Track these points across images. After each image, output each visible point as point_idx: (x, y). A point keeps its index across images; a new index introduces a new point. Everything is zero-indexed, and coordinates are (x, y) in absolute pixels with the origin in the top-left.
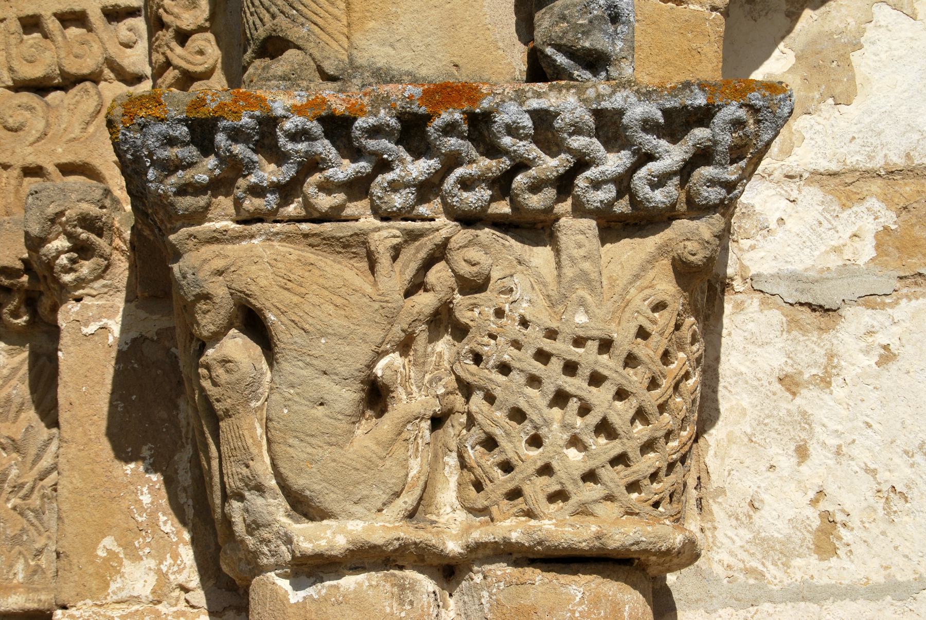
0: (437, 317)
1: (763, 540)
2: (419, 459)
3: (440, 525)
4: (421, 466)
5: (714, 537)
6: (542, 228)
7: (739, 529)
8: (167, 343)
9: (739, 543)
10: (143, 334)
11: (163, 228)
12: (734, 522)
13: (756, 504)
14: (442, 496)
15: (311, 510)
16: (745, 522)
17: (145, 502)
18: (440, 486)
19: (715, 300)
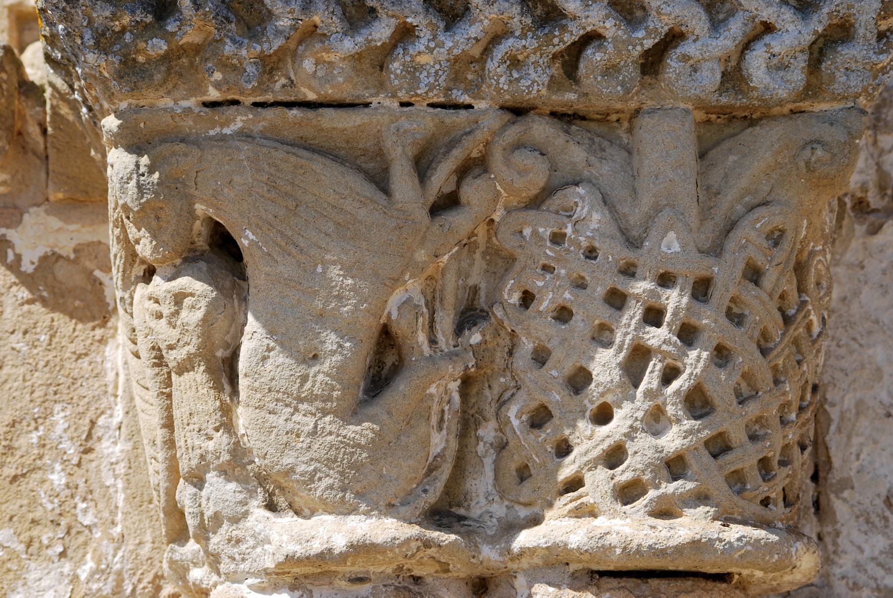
0: (473, 239)
2: (444, 432)
3: (471, 523)
4: (447, 441)
5: (835, 544)
6: (618, 120)
7: (870, 534)
8: (89, 265)
9: (867, 553)
10: (56, 250)
11: (96, 107)
12: (865, 527)
14: (474, 482)
15: (296, 499)
17: (56, 483)
18: (471, 470)
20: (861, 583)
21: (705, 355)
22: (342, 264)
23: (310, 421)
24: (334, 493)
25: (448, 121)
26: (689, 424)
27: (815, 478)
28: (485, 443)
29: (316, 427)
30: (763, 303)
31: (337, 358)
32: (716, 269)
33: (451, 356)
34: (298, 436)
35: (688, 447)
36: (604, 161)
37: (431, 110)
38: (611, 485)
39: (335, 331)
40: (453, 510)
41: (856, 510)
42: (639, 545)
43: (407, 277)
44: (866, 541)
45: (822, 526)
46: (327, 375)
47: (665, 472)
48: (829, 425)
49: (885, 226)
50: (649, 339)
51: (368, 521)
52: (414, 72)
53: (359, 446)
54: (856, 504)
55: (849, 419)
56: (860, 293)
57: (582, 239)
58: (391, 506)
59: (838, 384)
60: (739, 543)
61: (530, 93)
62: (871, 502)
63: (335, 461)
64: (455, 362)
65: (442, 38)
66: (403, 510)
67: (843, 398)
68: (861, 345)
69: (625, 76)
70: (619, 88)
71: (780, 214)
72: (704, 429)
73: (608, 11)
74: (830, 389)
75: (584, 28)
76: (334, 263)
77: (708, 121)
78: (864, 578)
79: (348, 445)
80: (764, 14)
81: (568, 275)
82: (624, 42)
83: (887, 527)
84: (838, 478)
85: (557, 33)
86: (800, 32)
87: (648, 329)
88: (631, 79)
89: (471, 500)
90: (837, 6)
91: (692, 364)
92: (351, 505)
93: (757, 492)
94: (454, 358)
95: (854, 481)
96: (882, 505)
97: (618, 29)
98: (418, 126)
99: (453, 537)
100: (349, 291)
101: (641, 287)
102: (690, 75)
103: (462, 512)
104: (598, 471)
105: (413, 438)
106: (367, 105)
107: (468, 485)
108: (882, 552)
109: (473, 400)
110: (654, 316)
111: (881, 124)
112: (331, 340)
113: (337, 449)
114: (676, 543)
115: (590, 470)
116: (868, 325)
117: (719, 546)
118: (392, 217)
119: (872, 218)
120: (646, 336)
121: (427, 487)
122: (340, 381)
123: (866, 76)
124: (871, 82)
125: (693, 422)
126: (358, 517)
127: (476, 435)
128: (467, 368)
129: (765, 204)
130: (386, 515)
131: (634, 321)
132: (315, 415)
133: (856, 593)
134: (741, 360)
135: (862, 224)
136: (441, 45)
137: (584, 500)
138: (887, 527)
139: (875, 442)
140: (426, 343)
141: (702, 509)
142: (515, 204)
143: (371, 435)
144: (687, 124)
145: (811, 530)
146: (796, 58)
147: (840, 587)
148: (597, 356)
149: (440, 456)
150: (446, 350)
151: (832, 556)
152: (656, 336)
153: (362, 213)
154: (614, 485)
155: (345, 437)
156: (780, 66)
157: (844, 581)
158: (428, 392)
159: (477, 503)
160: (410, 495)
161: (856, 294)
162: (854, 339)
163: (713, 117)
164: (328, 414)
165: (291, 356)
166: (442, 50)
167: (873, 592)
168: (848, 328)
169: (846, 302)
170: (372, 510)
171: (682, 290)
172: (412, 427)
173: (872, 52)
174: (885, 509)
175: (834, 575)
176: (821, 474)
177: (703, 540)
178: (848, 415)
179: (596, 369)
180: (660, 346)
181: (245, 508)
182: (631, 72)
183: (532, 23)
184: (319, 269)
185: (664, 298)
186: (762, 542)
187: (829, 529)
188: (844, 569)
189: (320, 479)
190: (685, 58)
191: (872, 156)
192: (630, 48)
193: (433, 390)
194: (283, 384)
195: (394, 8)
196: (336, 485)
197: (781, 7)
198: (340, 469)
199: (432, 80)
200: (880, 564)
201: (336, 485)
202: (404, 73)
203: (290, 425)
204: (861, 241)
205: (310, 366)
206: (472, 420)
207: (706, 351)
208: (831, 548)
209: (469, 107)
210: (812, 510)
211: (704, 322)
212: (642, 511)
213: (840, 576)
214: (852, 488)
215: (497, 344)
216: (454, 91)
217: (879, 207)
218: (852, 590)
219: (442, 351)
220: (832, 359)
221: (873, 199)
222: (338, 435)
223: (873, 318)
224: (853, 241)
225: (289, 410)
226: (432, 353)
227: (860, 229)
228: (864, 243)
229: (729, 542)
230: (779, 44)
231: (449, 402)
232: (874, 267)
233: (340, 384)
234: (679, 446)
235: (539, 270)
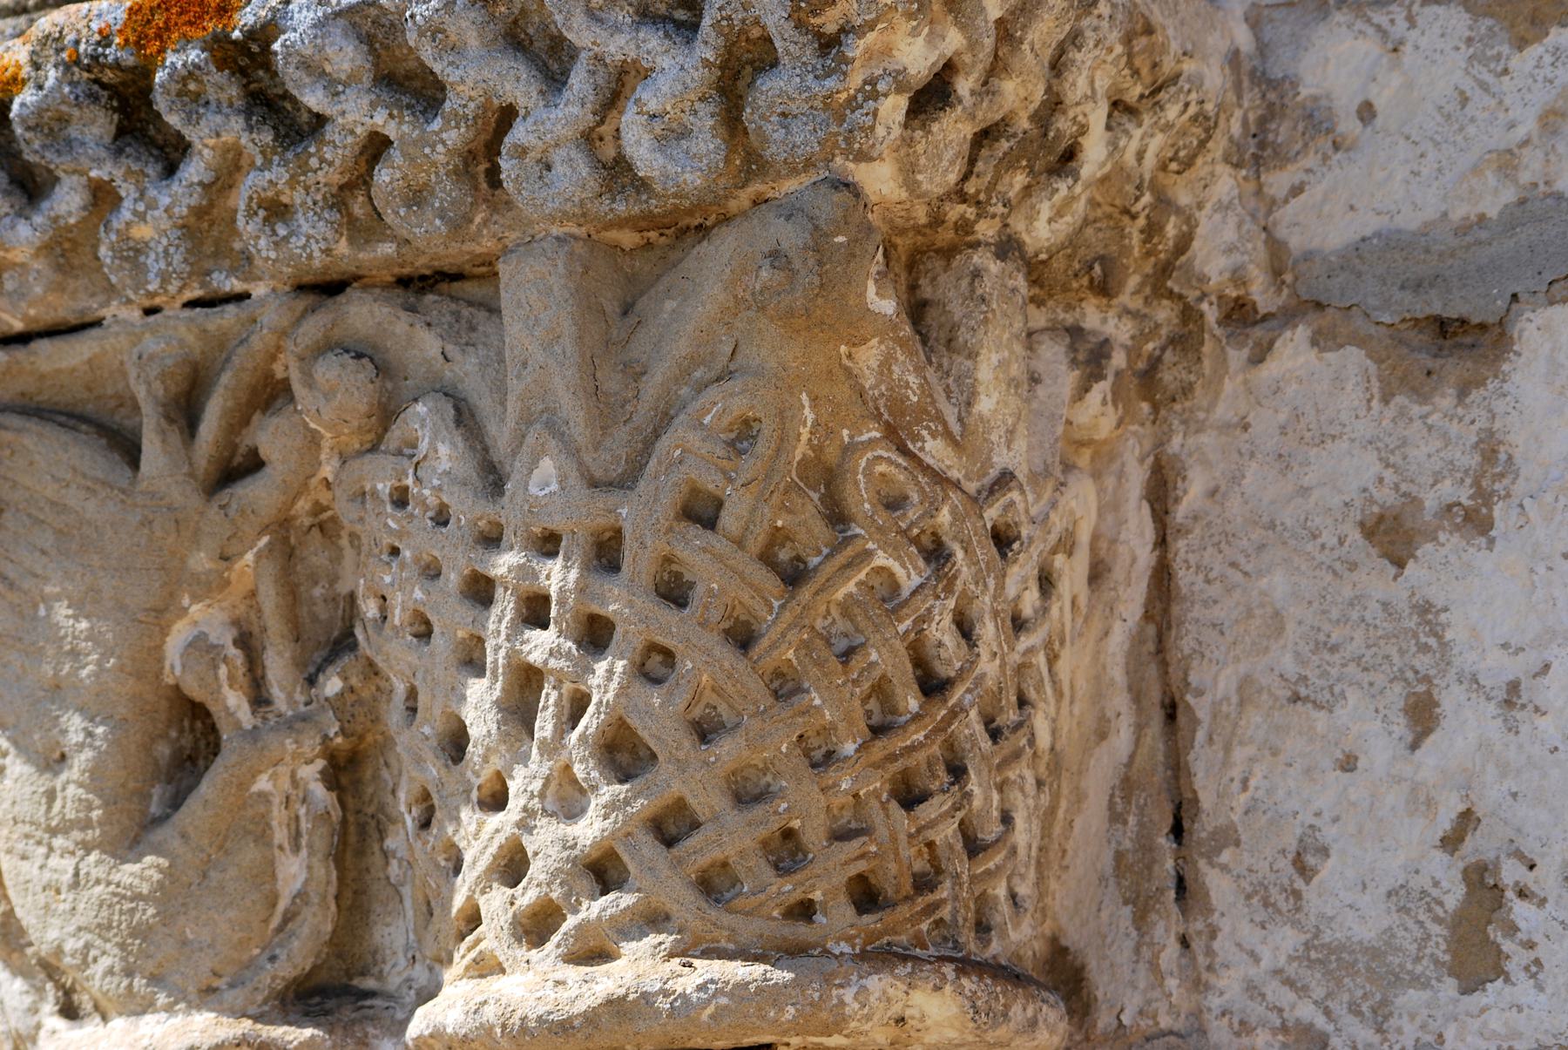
1: (1330, 949)
2: (304, 852)
4: (309, 868)
5: (1210, 952)
13: (1311, 860)
14: (387, 930)
16: (1284, 909)
19: (1202, 343)
20: (1253, 1021)
21: (620, 665)
22: (69, 598)
23: (68, 864)
24: (116, 980)
25: (211, 327)
26: (610, 791)
27: (1178, 831)
28: (400, 860)
29: (77, 874)
30: (719, 558)
31: (88, 754)
32: (624, 512)
33: (291, 725)
34: (58, 892)
35: (613, 833)
36: (471, 349)
37: (188, 313)
38: (510, 914)
39: (81, 710)
40: (355, 982)
41: (1244, 884)
42: (524, 1019)
43: (186, 601)
44: (1264, 941)
45: (1186, 921)
46: (80, 785)
47: (586, 883)
48: (1194, 731)
49: (1278, 344)
50: (529, 653)
51: (173, 1021)
52: (136, 257)
53: (138, 897)
54: (1246, 873)
55: (1227, 716)
56: (1244, 477)
57: (427, 492)
58: (211, 990)
59: (1207, 653)
60: (702, 995)
61: (310, 257)
62: (1271, 865)
63: (110, 927)
64: (299, 732)
65: (152, 193)
66: (229, 996)
67: (1215, 680)
68: (1246, 574)
69: (442, 200)
70: (438, 222)
71: (743, 392)
72: (635, 798)
73: (373, 97)
74: (1195, 663)
75: (352, 132)
76: (58, 598)
77: (649, 245)
78: (1261, 1010)
79: (124, 897)
80: (612, 49)
81: (417, 560)
82: (414, 143)
83: (1298, 909)
84: (1210, 829)
85: (312, 150)
86: (682, 68)
87: (528, 634)
88: (452, 203)
89: (384, 962)
90: (720, 9)
91: (599, 686)
92: (143, 998)
93: (762, 897)
94: (298, 725)
95: (1240, 829)
96: (1291, 870)
97: (400, 123)
98: (167, 344)
99: (308, 1032)
100: (87, 639)
101: (504, 564)
102: (540, 178)
103: (370, 983)
104: (494, 893)
105: (232, 872)
106: (97, 323)
107: (377, 936)
108: (1291, 959)
109: (370, 790)
110: (535, 612)
111: (1269, 151)
112: (74, 726)
113: (110, 906)
114: (583, 1008)
115: (483, 892)
116: (1257, 535)
117: (663, 1004)
118: (136, 505)
119: (1258, 332)
120: (526, 648)
121: (278, 951)
122: (99, 792)
123: (818, 120)
124: (834, 129)
125: (617, 787)
126: (156, 1017)
127: (382, 849)
128: (326, 738)
129: (725, 376)
130: (199, 1008)
131: (504, 624)
132: (73, 853)
133: (1245, 1040)
134: (690, 665)
135: (1241, 346)
136: (152, 205)
137: (482, 946)
138: (1298, 909)
139: (1275, 753)
140: (246, 707)
141: (652, 939)
142: (357, 446)
143: (157, 876)
144: (560, 265)
145: (1167, 930)
146: (696, 112)
147: (1219, 1031)
148: (468, 693)
149: (301, 896)
150: (290, 713)
151: (1205, 976)
152: (540, 645)
153: (91, 506)
154: (515, 915)
155: (118, 885)
156: (672, 135)
157: (1226, 1020)
158: (255, 788)
159: (394, 966)
160: (247, 967)
161: (1236, 479)
162: (1233, 565)
163: (653, 235)
164: (93, 849)
165: (28, 761)
166: (156, 213)
167: (1274, 1035)
168: (1223, 545)
169: (1218, 497)
170: (176, 1003)
171: (567, 558)
172: (227, 853)
173: (811, 76)
174: (1296, 876)
175: (1209, 1010)
176: (1186, 824)
177: (631, 997)
178: (1225, 708)
179: (469, 715)
180: (546, 662)
181: (36, 1018)
182: (446, 192)
183: (274, 140)
184: (42, 612)
185: (543, 577)
186: (752, 987)
187: (1199, 925)
188: (1226, 997)
189: (95, 960)
190: (521, 152)
191: (1253, 216)
192: (427, 150)
193: (263, 784)
194: (24, 809)
195: (62, 159)
196: (117, 969)
197: (637, 31)
198: (118, 939)
199: (162, 265)
200: (1289, 983)
201: (117, 969)
202: (117, 262)
203: (47, 875)
204: (1240, 378)
205: (56, 774)
206: (373, 823)
207: (622, 658)
208: (1202, 960)
209: (242, 297)
210: (1172, 894)
211: (611, 608)
212: (553, 956)
213: (1218, 1012)
214: (1237, 843)
215: (378, 689)
216: (215, 275)
217: (1273, 309)
218: (1238, 1034)
219: (280, 716)
220: (1197, 606)
221: (1262, 295)
222: (109, 884)
223: (1265, 519)
224: (1227, 380)
225: (42, 850)
226: (259, 722)
227: (1237, 357)
228: (1246, 382)
229: (683, 996)
230: (650, 97)
231: (304, 801)
232: (1265, 423)
233: (100, 797)
234: (598, 834)
235: (385, 557)
